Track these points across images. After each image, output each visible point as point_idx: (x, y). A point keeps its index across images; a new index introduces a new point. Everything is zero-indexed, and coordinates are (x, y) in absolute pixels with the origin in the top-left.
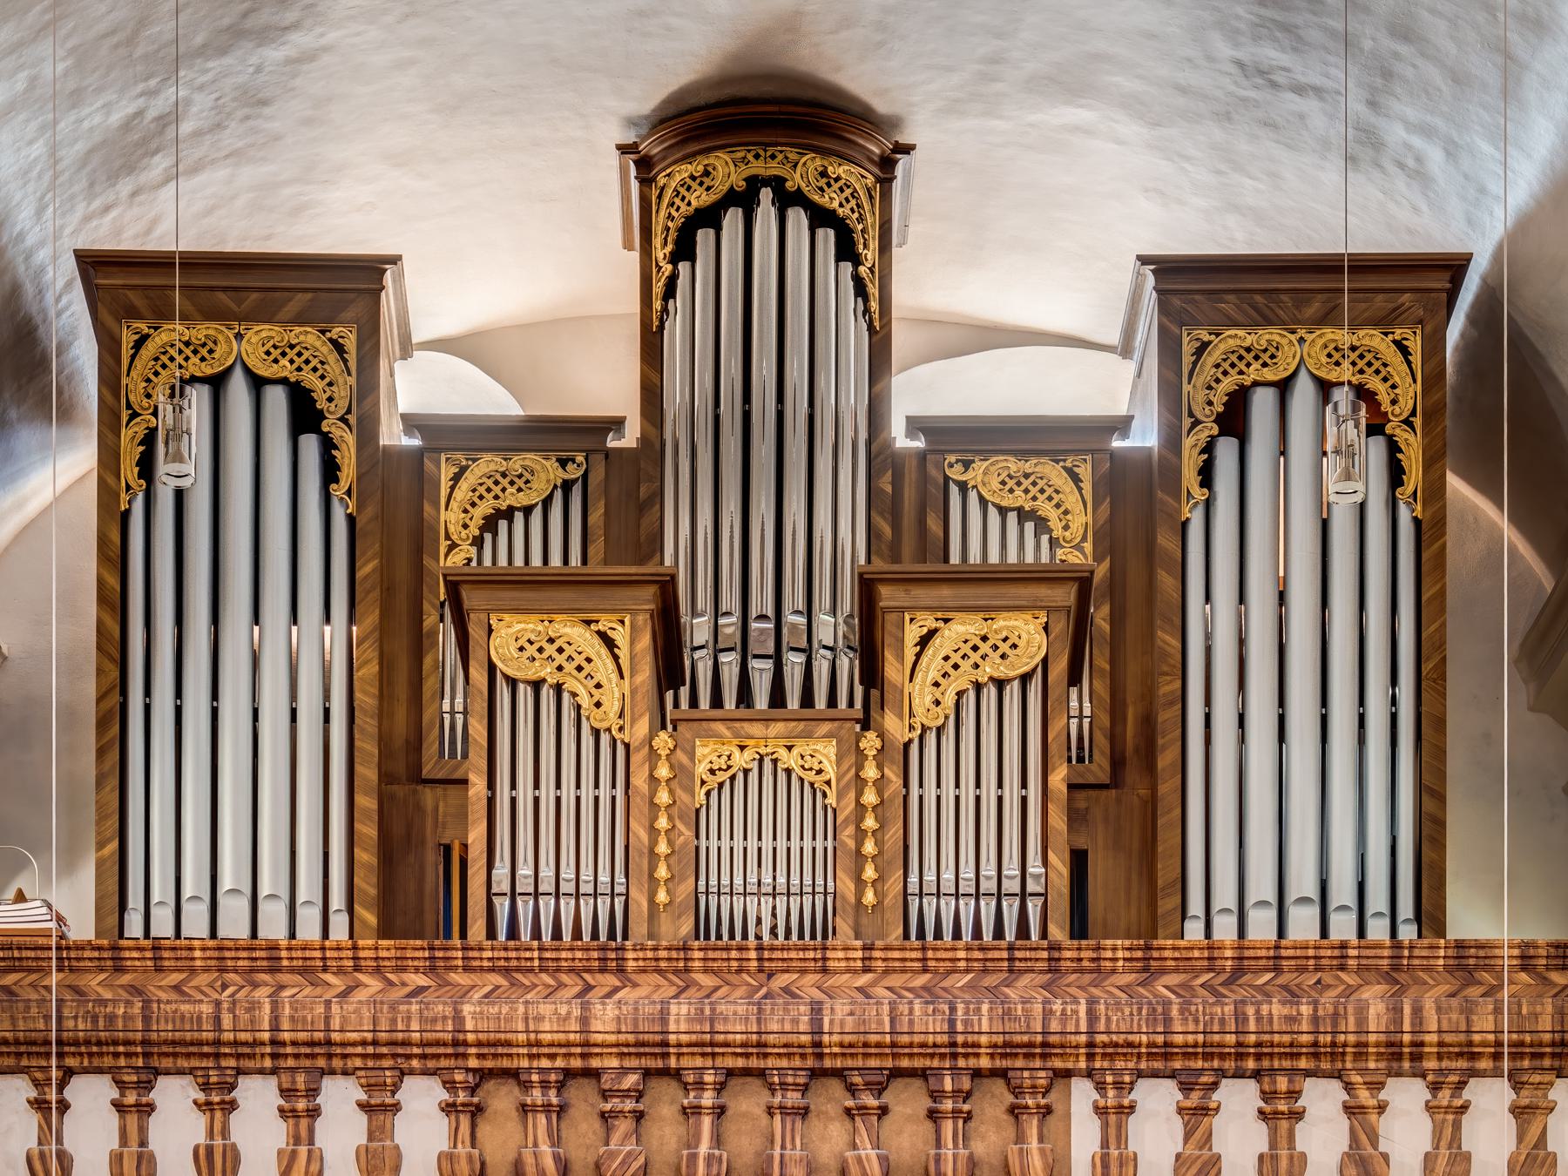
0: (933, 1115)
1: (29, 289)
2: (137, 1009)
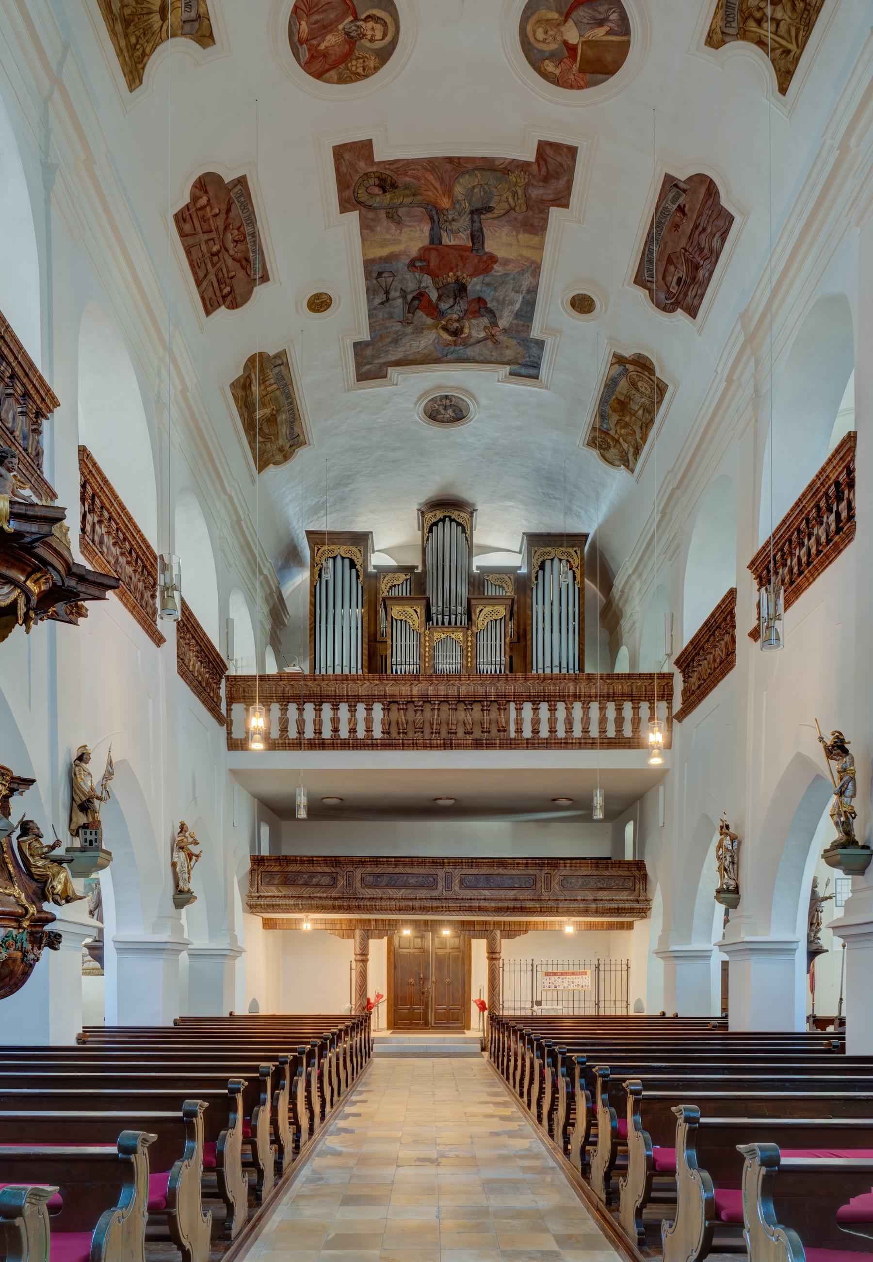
0: (482, 710)
1: (296, 539)
2: (319, 689)
